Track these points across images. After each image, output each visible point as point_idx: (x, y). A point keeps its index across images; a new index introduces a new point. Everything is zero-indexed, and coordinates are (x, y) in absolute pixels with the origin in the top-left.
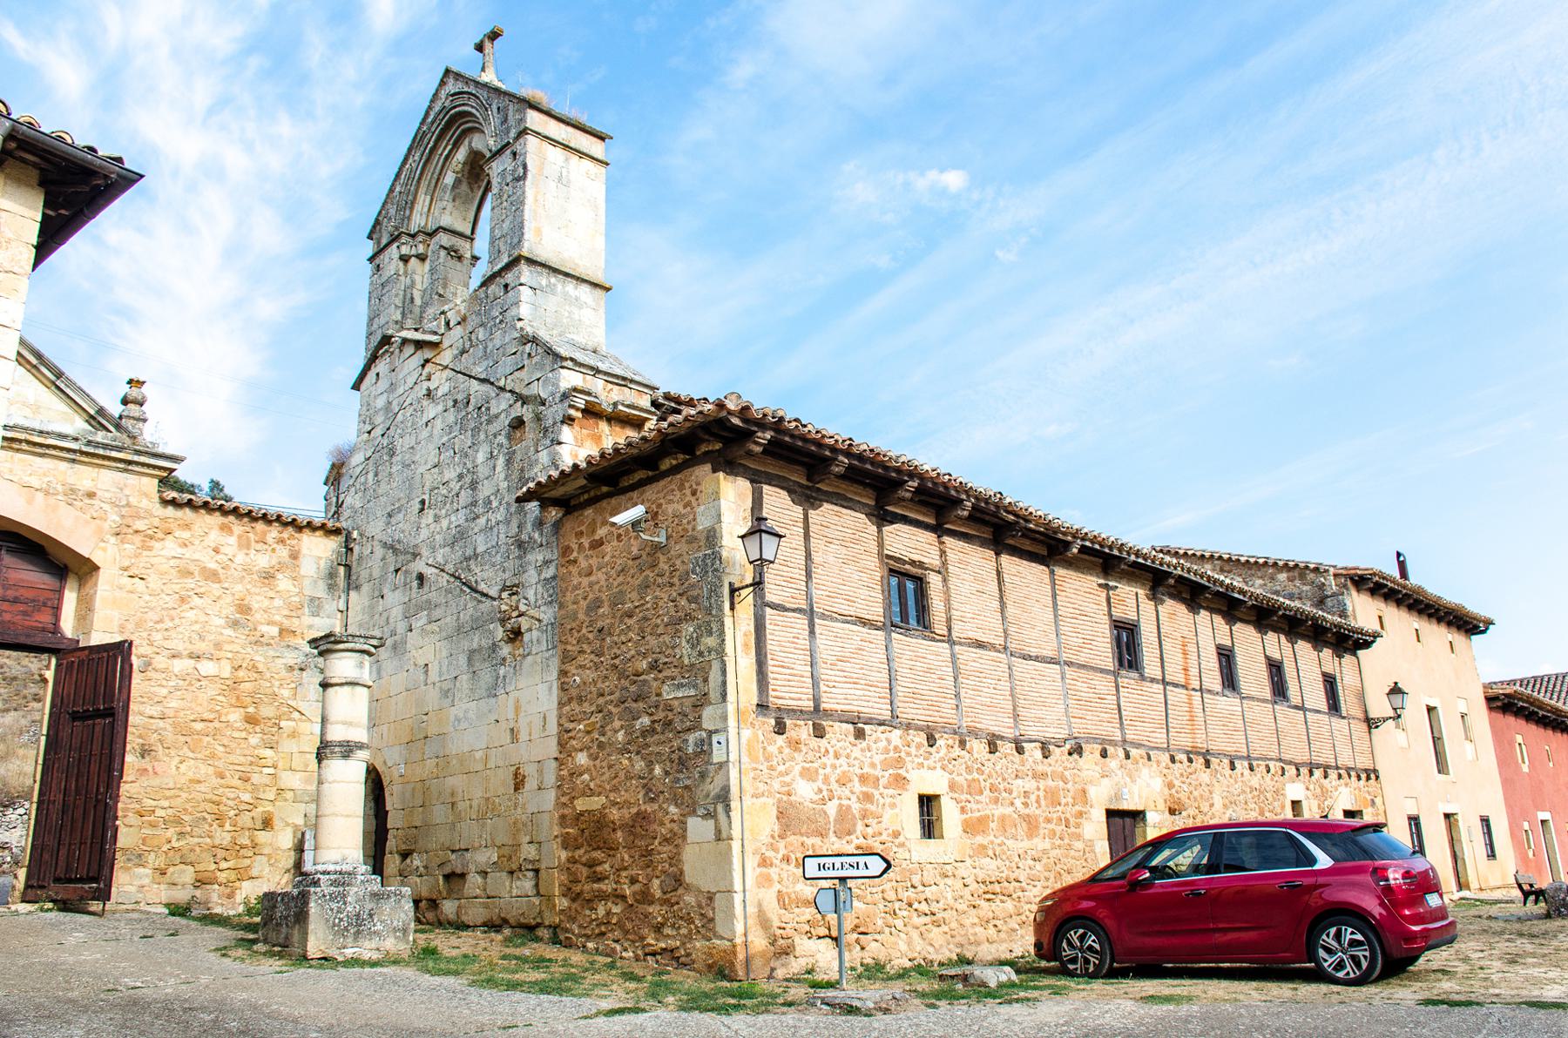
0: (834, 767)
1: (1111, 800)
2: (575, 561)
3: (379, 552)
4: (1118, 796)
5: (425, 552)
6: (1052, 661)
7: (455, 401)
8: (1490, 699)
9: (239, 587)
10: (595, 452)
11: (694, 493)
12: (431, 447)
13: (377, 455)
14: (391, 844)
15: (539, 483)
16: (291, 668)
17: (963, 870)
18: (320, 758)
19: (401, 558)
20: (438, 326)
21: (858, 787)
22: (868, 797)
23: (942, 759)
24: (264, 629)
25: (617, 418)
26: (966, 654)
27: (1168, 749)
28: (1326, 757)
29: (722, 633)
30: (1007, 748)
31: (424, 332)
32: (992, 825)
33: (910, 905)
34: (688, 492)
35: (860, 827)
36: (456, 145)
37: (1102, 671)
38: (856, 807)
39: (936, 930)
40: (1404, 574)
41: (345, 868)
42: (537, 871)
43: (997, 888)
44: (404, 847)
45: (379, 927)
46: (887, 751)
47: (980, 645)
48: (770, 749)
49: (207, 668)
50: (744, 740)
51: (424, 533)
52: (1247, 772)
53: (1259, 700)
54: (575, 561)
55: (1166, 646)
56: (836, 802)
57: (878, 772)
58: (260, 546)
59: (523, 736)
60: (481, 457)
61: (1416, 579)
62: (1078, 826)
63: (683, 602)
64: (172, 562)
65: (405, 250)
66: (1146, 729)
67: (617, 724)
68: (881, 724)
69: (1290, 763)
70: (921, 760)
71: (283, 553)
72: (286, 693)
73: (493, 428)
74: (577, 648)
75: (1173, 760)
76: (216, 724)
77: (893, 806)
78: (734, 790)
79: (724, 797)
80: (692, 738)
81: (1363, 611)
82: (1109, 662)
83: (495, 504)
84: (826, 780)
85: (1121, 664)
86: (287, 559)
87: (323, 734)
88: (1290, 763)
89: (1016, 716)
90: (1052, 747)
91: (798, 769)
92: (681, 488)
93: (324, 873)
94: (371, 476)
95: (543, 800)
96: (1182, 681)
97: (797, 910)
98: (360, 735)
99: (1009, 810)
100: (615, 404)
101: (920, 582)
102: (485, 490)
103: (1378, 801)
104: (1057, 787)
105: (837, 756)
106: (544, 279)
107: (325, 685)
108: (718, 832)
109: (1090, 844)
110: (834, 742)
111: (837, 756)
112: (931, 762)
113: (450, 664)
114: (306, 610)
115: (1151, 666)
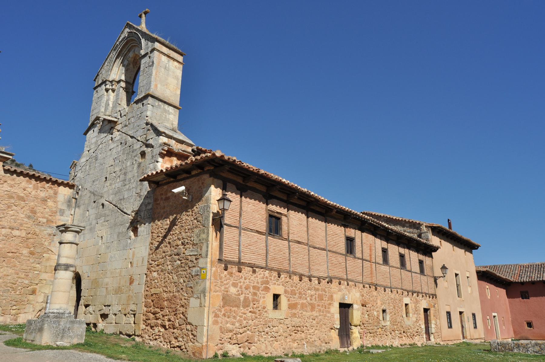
0: (244, 283)
1: (341, 300)
2: (159, 204)
3: (89, 195)
4: (344, 298)
5: (105, 196)
6: (324, 250)
7: (121, 143)
8: (478, 273)
9: (32, 204)
10: (169, 166)
11: (203, 183)
12: (111, 158)
13: (91, 159)
14: (82, 302)
15: (148, 175)
16: (50, 235)
17: (287, 322)
18: (55, 270)
19: (96, 197)
20: (118, 115)
21: (252, 290)
22: (255, 294)
23: (282, 282)
24: (41, 219)
25: (181, 156)
26: (294, 246)
27: (362, 283)
28: (418, 289)
29: (208, 233)
30: (306, 279)
31: (112, 117)
32: (299, 306)
33: (267, 333)
34: (201, 183)
35: (252, 305)
36: (129, 51)
37: (341, 254)
38: (250, 297)
39: (276, 343)
40: (450, 227)
41: (61, 311)
42: (134, 315)
43: (299, 329)
44: (87, 303)
45: (71, 334)
46: (263, 278)
47: (299, 242)
48: (222, 275)
49: (16, 233)
50: (212, 272)
51: (106, 189)
52: (390, 292)
53: (395, 268)
54: (159, 204)
55: (364, 247)
56: (244, 295)
57: (259, 285)
58: (41, 189)
59: (135, 265)
60: (129, 164)
61: (454, 230)
62: (329, 308)
63: (196, 221)
64: (6, 193)
65: (108, 87)
66: (355, 275)
67: (169, 263)
68: (262, 268)
69: (405, 290)
70: (275, 282)
71: (51, 192)
72: (46, 243)
73: (134, 154)
74: (156, 235)
75: (364, 287)
76: (17, 254)
77: (264, 297)
78: (208, 289)
79: (204, 292)
80: (194, 269)
81: (435, 241)
82: (343, 251)
83: (132, 181)
84: (241, 287)
85: (348, 252)
86: (52, 194)
87: (58, 260)
88: (405, 290)
89: (309, 268)
90: (321, 280)
91: (231, 282)
92: (199, 181)
93: (52, 313)
94: (88, 167)
95: (140, 288)
96: (369, 259)
97: (226, 334)
98: (70, 262)
99: (305, 301)
100: (178, 149)
101: (279, 219)
102: (129, 176)
103: (436, 306)
104: (322, 294)
105: (245, 279)
106: (157, 103)
107: (61, 243)
108: (201, 303)
109: (333, 315)
110: (245, 274)
111: (245, 279)
112: (278, 283)
113: (111, 237)
114: (58, 214)
115: (358, 254)
